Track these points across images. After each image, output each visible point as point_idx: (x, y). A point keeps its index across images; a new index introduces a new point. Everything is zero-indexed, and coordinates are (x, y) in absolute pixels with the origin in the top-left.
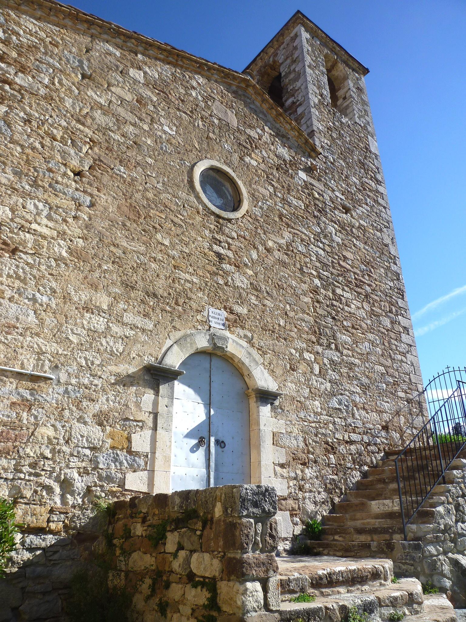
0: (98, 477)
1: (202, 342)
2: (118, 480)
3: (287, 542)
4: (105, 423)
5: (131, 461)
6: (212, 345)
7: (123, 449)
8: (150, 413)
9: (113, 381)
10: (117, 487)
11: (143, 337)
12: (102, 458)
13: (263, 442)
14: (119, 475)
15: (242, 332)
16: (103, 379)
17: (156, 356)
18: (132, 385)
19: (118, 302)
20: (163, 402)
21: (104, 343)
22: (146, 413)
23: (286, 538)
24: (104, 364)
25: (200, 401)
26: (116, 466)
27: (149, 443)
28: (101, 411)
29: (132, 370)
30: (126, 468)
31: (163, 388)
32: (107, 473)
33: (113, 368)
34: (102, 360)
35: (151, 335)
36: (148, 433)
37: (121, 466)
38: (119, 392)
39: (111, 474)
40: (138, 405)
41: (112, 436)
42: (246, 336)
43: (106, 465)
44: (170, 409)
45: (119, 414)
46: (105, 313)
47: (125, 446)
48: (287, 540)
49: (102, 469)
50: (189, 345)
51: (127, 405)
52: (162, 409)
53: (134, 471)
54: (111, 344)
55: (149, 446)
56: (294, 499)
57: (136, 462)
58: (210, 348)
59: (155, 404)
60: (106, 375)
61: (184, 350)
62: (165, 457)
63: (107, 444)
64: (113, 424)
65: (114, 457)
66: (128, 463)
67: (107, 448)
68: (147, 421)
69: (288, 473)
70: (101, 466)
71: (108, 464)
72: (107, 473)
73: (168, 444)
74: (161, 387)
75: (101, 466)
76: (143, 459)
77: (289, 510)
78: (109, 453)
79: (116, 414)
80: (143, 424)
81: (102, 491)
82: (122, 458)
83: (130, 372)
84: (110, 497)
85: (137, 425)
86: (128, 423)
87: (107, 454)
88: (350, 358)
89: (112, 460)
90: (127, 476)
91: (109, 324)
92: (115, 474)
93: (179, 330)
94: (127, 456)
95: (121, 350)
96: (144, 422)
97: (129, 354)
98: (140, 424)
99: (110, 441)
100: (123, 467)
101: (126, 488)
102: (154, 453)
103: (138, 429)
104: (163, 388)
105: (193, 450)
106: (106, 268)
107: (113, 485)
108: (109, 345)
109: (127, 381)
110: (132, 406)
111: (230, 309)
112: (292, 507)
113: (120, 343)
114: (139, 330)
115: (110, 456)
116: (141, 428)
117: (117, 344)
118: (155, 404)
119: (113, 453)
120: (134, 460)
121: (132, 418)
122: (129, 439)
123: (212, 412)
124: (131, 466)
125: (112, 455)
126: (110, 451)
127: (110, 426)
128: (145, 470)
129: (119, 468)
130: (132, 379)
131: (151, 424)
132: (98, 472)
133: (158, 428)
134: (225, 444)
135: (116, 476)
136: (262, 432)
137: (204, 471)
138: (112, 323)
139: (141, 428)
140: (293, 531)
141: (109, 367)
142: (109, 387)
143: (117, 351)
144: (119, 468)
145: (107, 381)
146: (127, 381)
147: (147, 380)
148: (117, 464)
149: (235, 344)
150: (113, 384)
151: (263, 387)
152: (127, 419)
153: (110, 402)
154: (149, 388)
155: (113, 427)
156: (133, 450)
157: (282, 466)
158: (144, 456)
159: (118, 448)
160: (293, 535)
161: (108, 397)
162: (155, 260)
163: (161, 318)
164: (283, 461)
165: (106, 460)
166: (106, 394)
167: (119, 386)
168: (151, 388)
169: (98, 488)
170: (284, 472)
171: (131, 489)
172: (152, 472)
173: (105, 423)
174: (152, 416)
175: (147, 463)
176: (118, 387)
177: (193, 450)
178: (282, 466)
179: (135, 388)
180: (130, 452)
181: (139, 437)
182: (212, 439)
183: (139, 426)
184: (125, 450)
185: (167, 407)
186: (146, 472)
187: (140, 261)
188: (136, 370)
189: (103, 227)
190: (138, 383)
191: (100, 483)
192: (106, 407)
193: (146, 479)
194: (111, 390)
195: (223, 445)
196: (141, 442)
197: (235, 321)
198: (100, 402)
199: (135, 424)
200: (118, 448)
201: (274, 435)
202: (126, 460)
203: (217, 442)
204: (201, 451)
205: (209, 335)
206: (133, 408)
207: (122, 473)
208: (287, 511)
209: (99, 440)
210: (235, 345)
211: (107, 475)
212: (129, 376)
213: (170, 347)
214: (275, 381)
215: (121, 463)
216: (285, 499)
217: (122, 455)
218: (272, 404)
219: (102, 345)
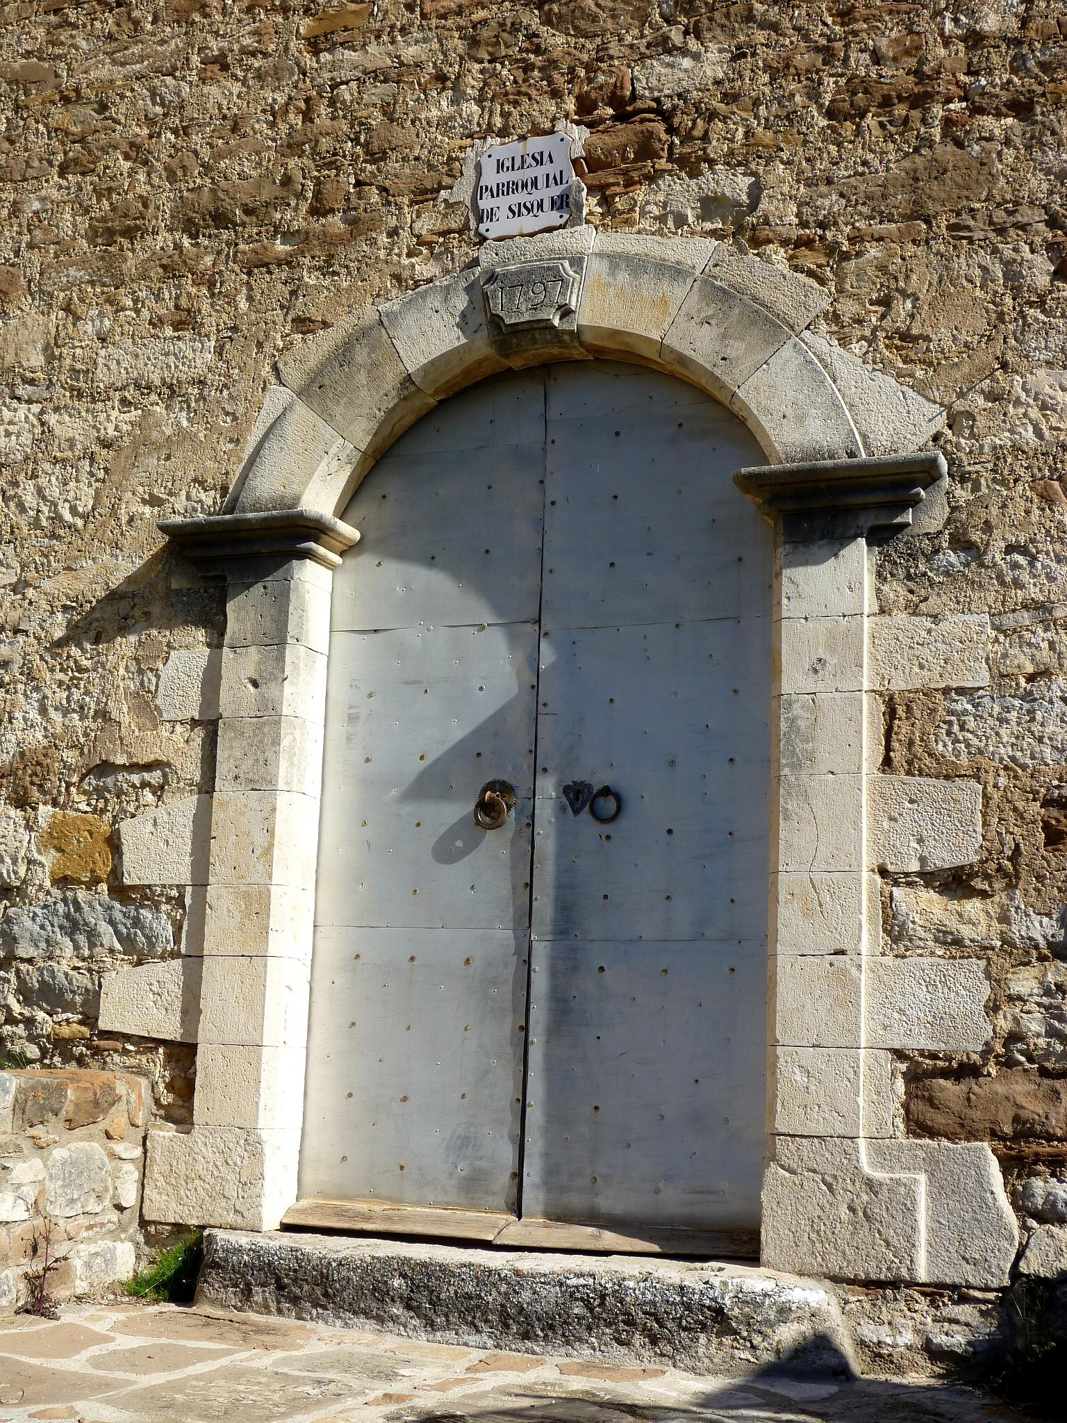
0: (18, 991)
1: (431, 335)
2: (78, 999)
3: (966, 1312)
4: (35, 794)
5: (128, 922)
6: (483, 337)
7: (96, 881)
8: (194, 723)
9: (58, 633)
10: (81, 1023)
11: (170, 420)
12: (28, 923)
13: (796, 766)
14: (82, 980)
15: (680, 191)
16: (25, 632)
17: (220, 480)
18: (123, 630)
19: (77, 318)
20: (238, 667)
21: (30, 499)
22: (179, 728)
23: (954, 1287)
24: (31, 575)
25: (487, 617)
26: (77, 947)
27: (188, 849)
28: (22, 754)
29: (123, 567)
30: (112, 951)
31: (241, 612)
32: (42, 975)
33: (59, 585)
34: (24, 566)
35: (202, 398)
36: (183, 806)
37: (92, 946)
38: (81, 670)
39: (54, 978)
40: (145, 705)
41: (56, 839)
42: (710, 205)
43: (43, 945)
44: (270, 690)
45: (82, 754)
46: (32, 382)
47: (103, 871)
48: (964, 1299)
49: (30, 961)
50: (362, 378)
51: (103, 714)
52: (236, 696)
53: (139, 963)
54: (54, 492)
55: (188, 860)
56: (1044, 1072)
57: (142, 928)
58: (483, 348)
59: (211, 680)
60: (36, 617)
61: (338, 410)
62: (246, 896)
63: (39, 870)
64: (59, 793)
65: (67, 916)
66: (117, 932)
67: (41, 887)
68: (177, 762)
69: (1004, 919)
70: (24, 950)
71: (47, 941)
72: (42, 975)
73: (260, 839)
74: (230, 607)
75: (24, 950)
76: (169, 915)
77: (994, 1135)
78: (51, 900)
79: (70, 756)
80: (165, 776)
81: (32, 1039)
82: (94, 917)
83: (116, 581)
84: (57, 1059)
85: (144, 784)
86: (109, 781)
87: (45, 907)
88: (814, 109)
89: (61, 927)
90: (109, 979)
91: (45, 417)
92: (66, 974)
93: (325, 325)
94: (111, 908)
95: (86, 504)
96: (168, 764)
97: (114, 510)
98: (155, 777)
99: (48, 859)
100: (98, 949)
101: (103, 1024)
102: (201, 884)
103: (148, 796)
104: (239, 609)
105: (446, 852)
106: (36, 205)
107: (64, 1016)
108: (44, 498)
109: (103, 620)
110: (122, 711)
111: (615, 100)
112: (1016, 1119)
113: (84, 477)
114: (154, 397)
115: (55, 913)
116: (158, 791)
117: (72, 484)
118: (211, 680)
119: (65, 900)
120: (137, 922)
121: (121, 760)
122: (114, 843)
123: (548, 655)
124: (128, 943)
125: (61, 908)
126: (56, 892)
127: (55, 803)
128: (175, 955)
129: (86, 953)
130: (124, 606)
131: (192, 769)
132: (18, 971)
133: (218, 783)
134: (618, 798)
135: (70, 983)
136: (797, 710)
137: (505, 936)
138: (56, 409)
139: (158, 791)
140: (1020, 1255)
141: (47, 585)
142: (48, 658)
143: (74, 511)
144: (86, 953)
145: (38, 639)
146: (103, 620)
147: (178, 592)
148: (82, 939)
149: (623, 276)
150: (60, 643)
151: (818, 453)
152: (105, 768)
153: (52, 714)
154: (186, 623)
155: (63, 807)
156: (127, 881)
157: (955, 883)
158: (169, 899)
159: (80, 882)
160: (1015, 1273)
161: (45, 697)
162: (225, 67)
163: (243, 305)
164: (959, 849)
165: (42, 927)
166: (37, 689)
167: (79, 645)
168: (196, 624)
169: (20, 1030)
170: (975, 917)
171: (117, 1027)
172: (194, 960)
173: (35, 794)
174: (198, 735)
175: (181, 928)
176: (75, 651)
177: (446, 852)
178: (955, 883)
179: (133, 639)
180: (120, 891)
181: (150, 827)
182: (548, 788)
183: (149, 785)
184: (103, 887)
185: (255, 684)
186: (177, 964)
187: (163, 105)
188: (139, 563)
189: (28, 54)
190: (147, 614)
191: (27, 1012)
192: (39, 736)
193: (174, 990)
194: (52, 670)
195: (609, 805)
196: (155, 845)
197: (646, 150)
198: (19, 724)
199: (136, 778)
200: (80, 882)
201: (891, 713)
202: (112, 922)
203: (579, 797)
204: (496, 846)
205: (468, 290)
206: (126, 720)
207: (90, 970)
208: (972, 1135)
209: (15, 861)
210: (623, 277)
211: (42, 983)
212: (113, 596)
213: (274, 423)
214: (921, 388)
215: (92, 935)
216: (966, 1071)
217: (95, 904)
218: (880, 536)
219: (22, 508)
